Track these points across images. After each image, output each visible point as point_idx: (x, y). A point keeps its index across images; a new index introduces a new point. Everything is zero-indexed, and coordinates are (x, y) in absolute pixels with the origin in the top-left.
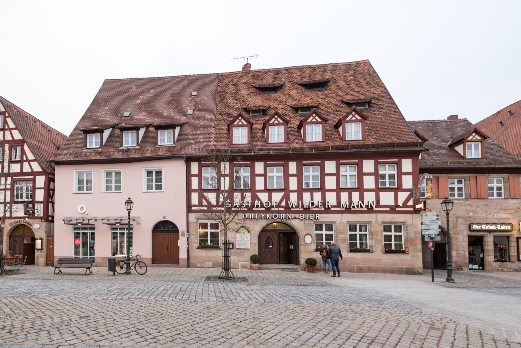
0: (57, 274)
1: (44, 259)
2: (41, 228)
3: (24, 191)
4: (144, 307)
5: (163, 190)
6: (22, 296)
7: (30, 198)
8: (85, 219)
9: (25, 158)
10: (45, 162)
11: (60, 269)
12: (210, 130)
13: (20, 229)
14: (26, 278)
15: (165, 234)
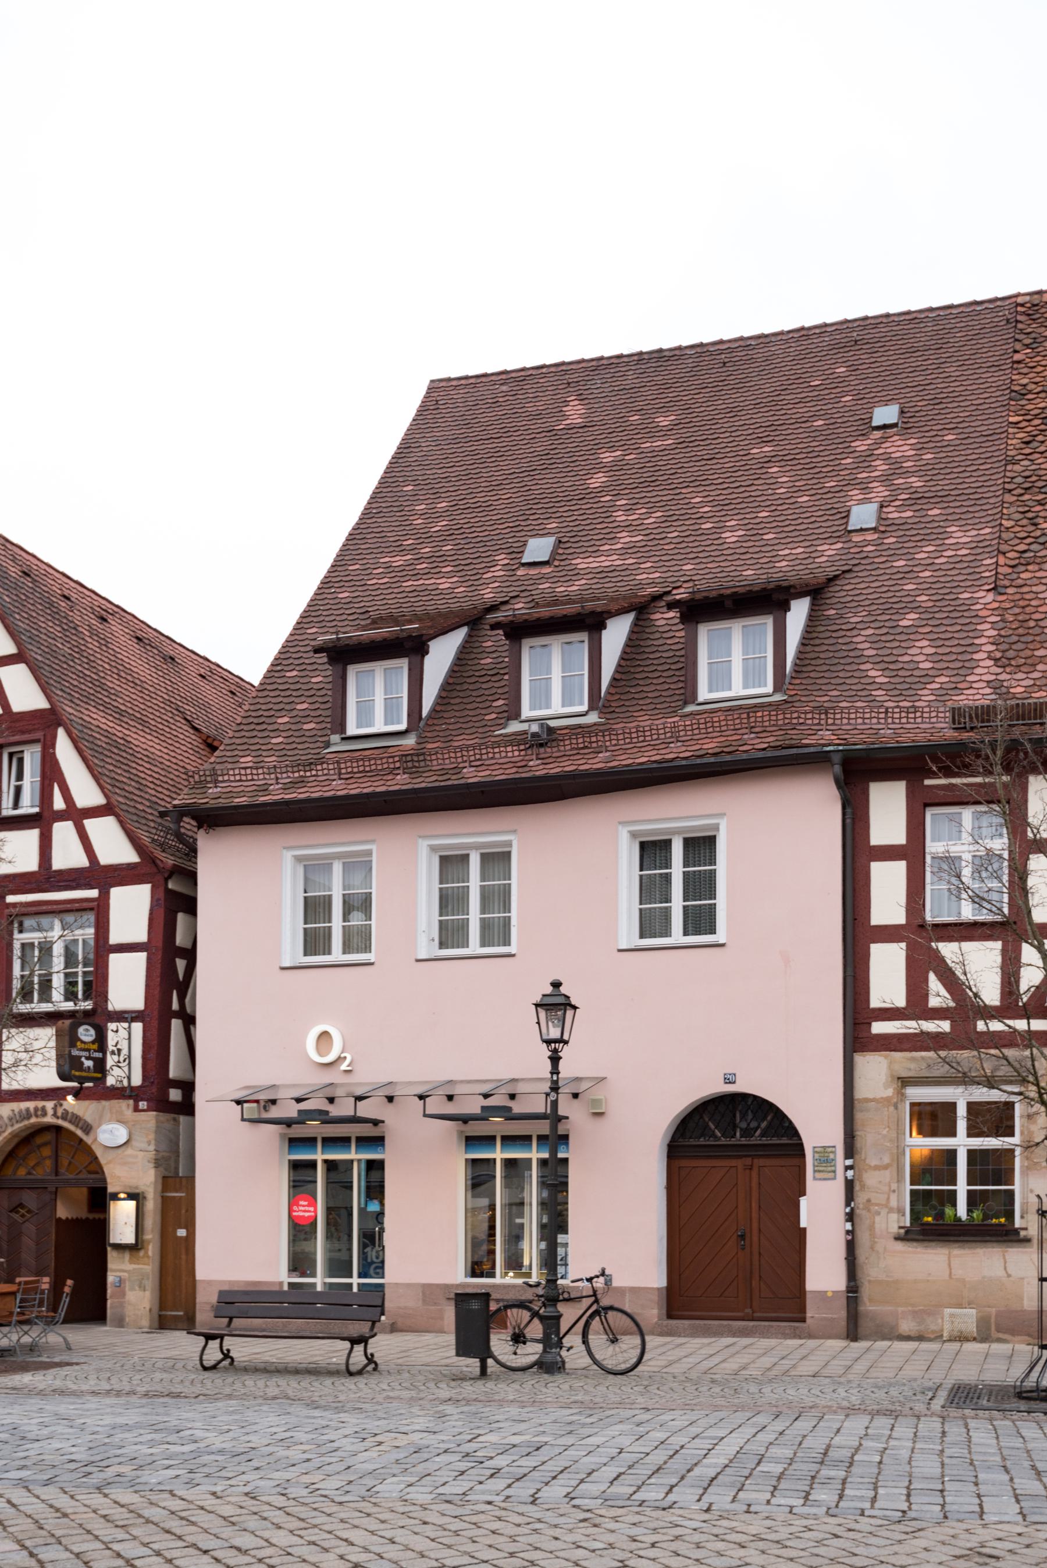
0: (214, 1367)
1: (148, 1294)
2: (134, 1143)
3: (58, 963)
4: (653, 1545)
5: (720, 936)
6: (67, 1477)
7: (86, 998)
8: (339, 1092)
9: (59, 803)
10: (152, 814)
11: (228, 1342)
12: (968, 605)
13: (39, 1147)
14: (74, 1387)
15: (733, 1162)
